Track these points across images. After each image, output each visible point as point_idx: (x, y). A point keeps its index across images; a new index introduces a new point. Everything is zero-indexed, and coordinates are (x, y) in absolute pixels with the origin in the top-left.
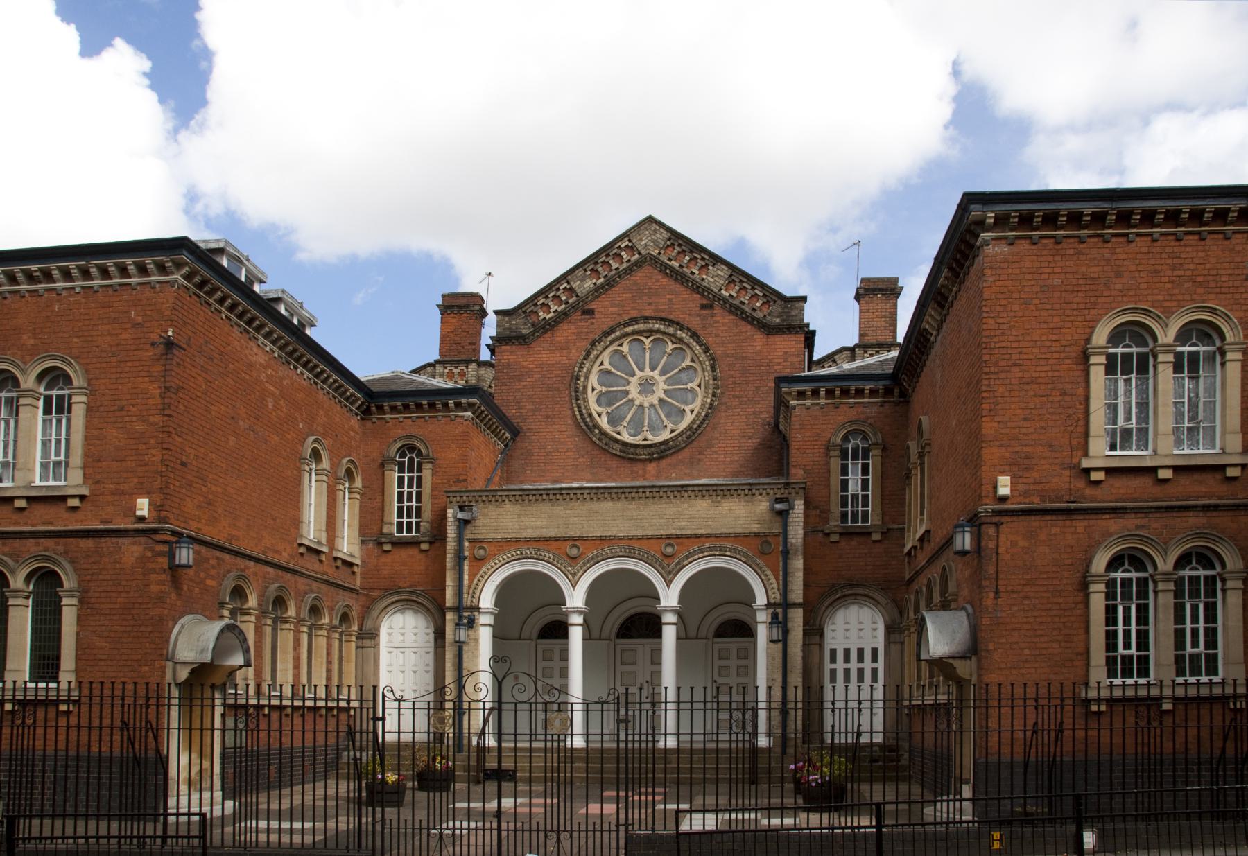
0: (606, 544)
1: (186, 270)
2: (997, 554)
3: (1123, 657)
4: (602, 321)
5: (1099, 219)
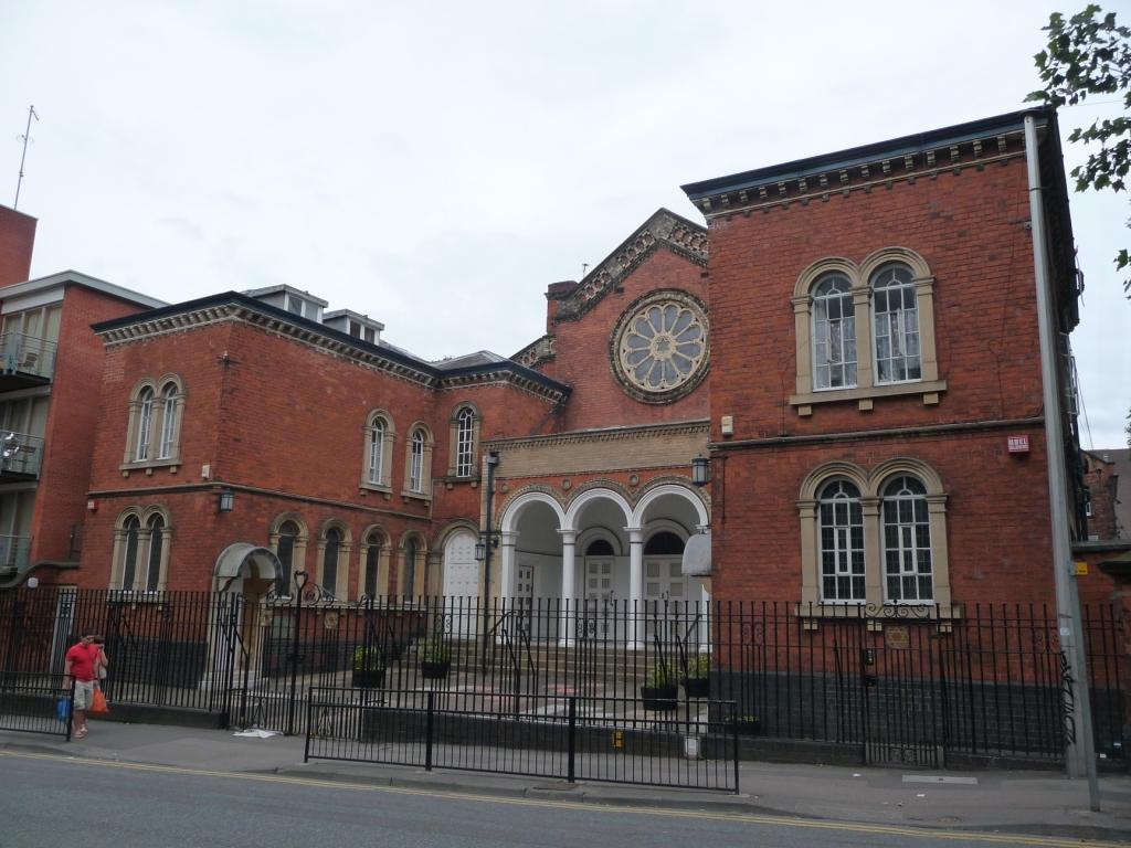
0: (587, 478)
1: (238, 311)
2: (724, 484)
3: (840, 578)
4: (629, 297)
5: (792, 188)
